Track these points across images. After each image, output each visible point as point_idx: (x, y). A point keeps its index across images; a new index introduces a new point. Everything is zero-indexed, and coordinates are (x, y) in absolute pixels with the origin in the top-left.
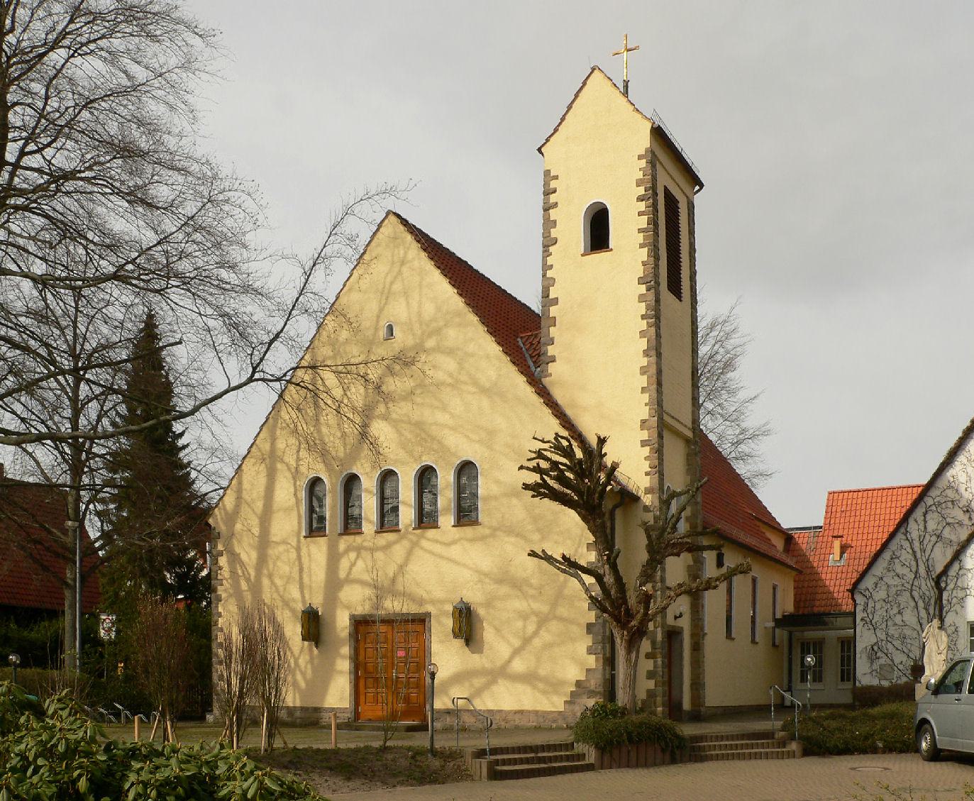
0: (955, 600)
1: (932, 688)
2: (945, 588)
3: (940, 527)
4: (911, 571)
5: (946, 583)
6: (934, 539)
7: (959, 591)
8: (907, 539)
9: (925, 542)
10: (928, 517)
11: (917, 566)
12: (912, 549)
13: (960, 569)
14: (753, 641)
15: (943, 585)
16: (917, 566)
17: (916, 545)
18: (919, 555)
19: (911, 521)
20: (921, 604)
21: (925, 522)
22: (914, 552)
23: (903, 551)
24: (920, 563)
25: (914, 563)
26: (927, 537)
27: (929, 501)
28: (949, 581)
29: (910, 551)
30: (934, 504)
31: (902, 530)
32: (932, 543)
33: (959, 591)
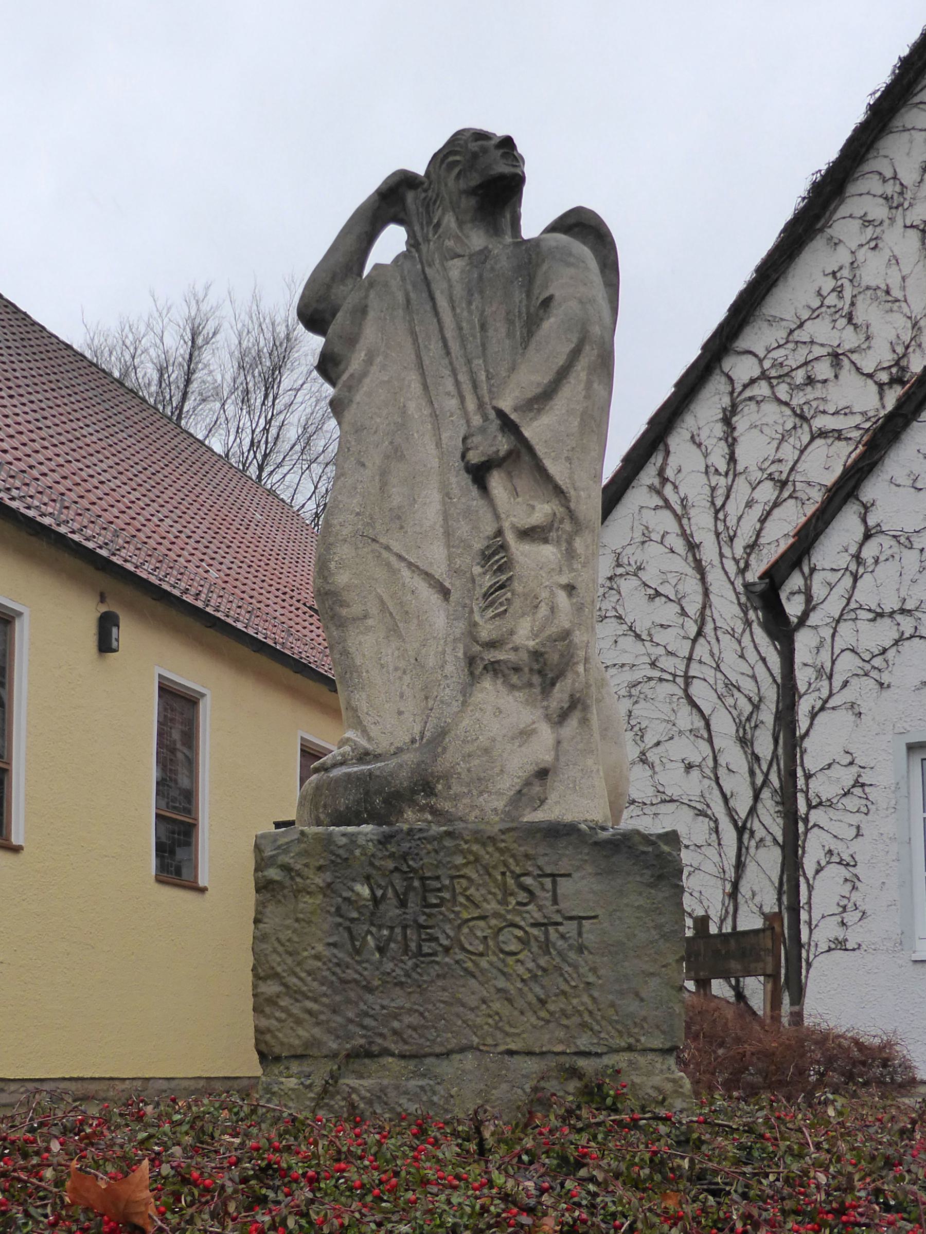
0: (847, 664)
1: (579, 707)
2: (803, 619)
3: (789, 453)
4: (684, 613)
5: (809, 598)
6: (767, 492)
7: (863, 626)
8: (667, 505)
9: (733, 509)
10: (741, 423)
11: (706, 593)
12: (685, 536)
13: (867, 536)
14: (175, 849)
15: (793, 608)
16: (706, 593)
17: (702, 523)
18: (709, 553)
19: (678, 441)
20: (724, 726)
21: (730, 440)
22: (693, 547)
23: (653, 549)
24: (715, 577)
25: (692, 586)
26: (742, 490)
27: (742, 368)
28: (818, 590)
29: (679, 545)
30: (764, 376)
31: (648, 476)
32: (757, 511)
33: (863, 626)
